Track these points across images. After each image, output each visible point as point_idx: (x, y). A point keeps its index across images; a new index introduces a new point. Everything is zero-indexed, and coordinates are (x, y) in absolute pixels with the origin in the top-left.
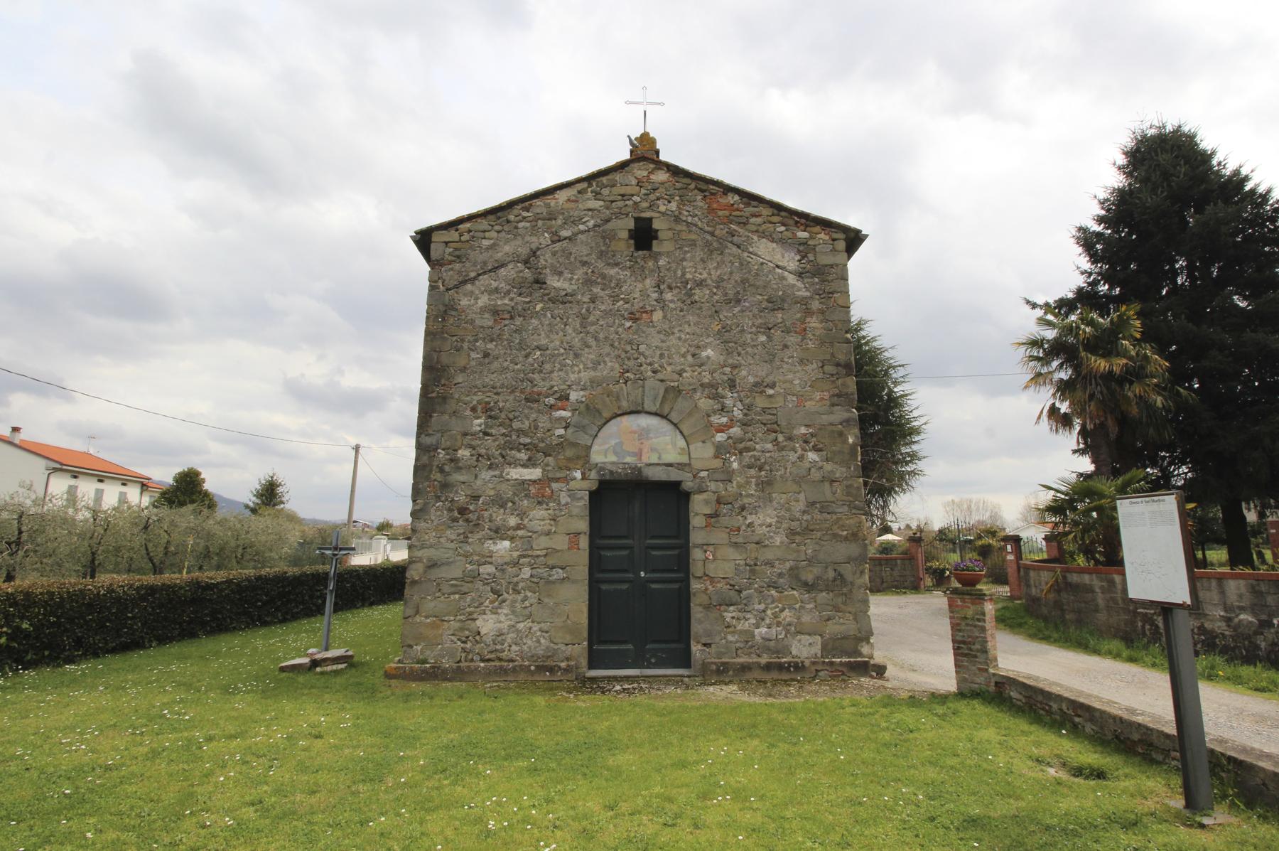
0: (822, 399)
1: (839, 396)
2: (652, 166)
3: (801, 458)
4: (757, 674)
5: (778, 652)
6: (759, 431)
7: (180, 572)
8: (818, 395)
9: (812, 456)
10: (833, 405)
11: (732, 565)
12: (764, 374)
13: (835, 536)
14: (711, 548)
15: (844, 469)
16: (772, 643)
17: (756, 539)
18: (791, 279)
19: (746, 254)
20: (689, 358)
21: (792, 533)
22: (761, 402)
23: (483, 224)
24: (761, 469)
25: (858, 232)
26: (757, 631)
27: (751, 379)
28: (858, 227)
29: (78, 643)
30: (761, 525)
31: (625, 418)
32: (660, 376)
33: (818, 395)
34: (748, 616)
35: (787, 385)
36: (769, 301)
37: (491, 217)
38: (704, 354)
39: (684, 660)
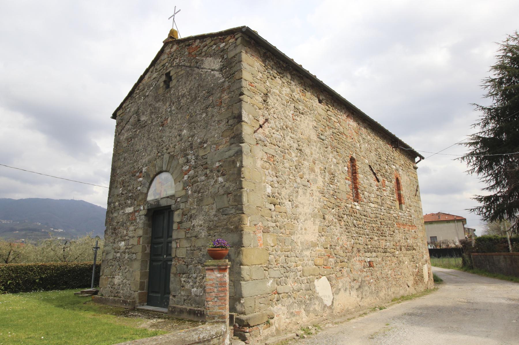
0: (226, 142)
1: (233, 137)
2: (171, 45)
3: (216, 182)
4: (185, 316)
5: (199, 304)
6: (200, 170)
7: (333, 262)
8: (224, 141)
9: (221, 179)
10: (231, 144)
11: (185, 250)
12: (203, 136)
13: (228, 229)
14: (178, 241)
15: (234, 185)
16: (197, 298)
17: (195, 234)
18: (217, 74)
19: (201, 70)
20: (178, 137)
21: (209, 229)
22: (201, 153)
23: (128, 102)
24: (199, 192)
25: (171, 30)
26: (193, 290)
27: (199, 141)
28: (243, 25)
29: (66, 283)
30: (197, 226)
31: (158, 177)
32: (169, 151)
33: (224, 141)
34: (190, 280)
35: (212, 139)
36: (208, 92)
37: (130, 98)
38: (183, 133)
39: (164, 303)
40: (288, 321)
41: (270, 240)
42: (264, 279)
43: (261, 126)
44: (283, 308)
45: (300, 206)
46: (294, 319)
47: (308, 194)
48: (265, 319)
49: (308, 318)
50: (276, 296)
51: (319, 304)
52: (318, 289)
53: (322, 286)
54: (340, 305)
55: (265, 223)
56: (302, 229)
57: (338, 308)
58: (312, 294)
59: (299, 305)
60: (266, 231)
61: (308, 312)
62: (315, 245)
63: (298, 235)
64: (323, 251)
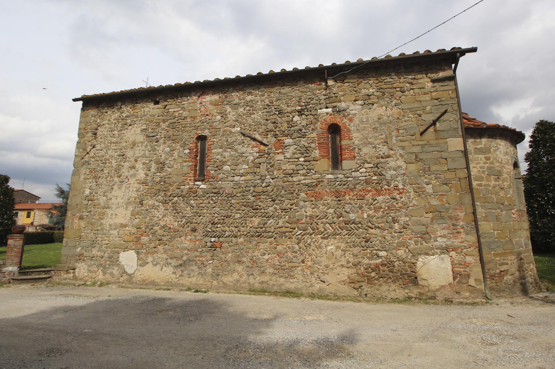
40: (86, 274)
41: (82, 224)
42: (75, 247)
43: (88, 153)
44: (85, 266)
45: (113, 198)
46: (90, 275)
47: (123, 188)
48: (66, 269)
49: (103, 277)
50: (80, 257)
51: (118, 270)
52: (121, 259)
53: (128, 259)
54: (142, 276)
55: (81, 214)
56: (112, 215)
57: (139, 277)
58: (114, 261)
59: (98, 266)
60: (81, 218)
61: (104, 273)
62: (124, 226)
63: (107, 220)
64: (134, 230)
